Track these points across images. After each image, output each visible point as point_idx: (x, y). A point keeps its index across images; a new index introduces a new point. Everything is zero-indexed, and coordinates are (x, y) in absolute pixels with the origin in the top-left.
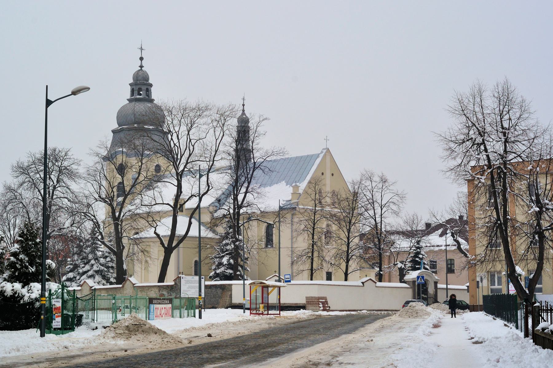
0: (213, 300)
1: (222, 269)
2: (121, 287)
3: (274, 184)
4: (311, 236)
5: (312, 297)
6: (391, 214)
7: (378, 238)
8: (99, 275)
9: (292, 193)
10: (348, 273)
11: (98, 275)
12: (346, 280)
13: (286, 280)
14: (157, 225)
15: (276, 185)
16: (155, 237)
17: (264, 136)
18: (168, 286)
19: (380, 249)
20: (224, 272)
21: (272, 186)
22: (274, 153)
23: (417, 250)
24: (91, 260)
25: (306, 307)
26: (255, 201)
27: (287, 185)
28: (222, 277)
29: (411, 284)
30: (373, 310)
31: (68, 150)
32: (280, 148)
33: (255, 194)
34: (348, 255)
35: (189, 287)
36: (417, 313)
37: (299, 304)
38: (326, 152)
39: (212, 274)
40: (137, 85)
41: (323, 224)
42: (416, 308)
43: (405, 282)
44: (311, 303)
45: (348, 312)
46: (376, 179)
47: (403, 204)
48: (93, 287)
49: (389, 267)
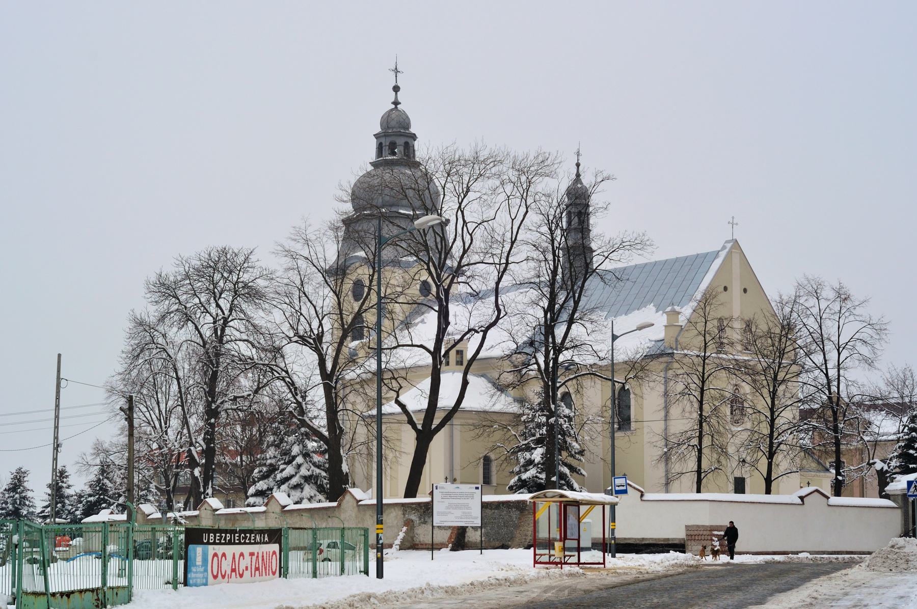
0: (504, 531)
1: (532, 472)
2: (335, 507)
3: (634, 310)
4: (696, 405)
5: (698, 526)
6: (857, 362)
7: (832, 408)
8: (311, 484)
9: (665, 326)
10: (773, 479)
11: (309, 484)
12: (768, 491)
13: (617, 488)
14: (401, 387)
15: (636, 311)
16: (399, 414)
17: (606, 212)
18: (419, 504)
19: (836, 429)
20: (536, 477)
21: (631, 313)
22: (624, 244)
23: (910, 433)
24: (296, 456)
25: (686, 547)
26: (590, 338)
27: (657, 311)
28: (532, 487)
29: (900, 501)
30: (824, 553)
31: (250, 251)
32: (635, 235)
33: (588, 325)
34: (771, 443)
35: (450, 506)
36: (907, 561)
37: (673, 539)
38: (732, 248)
39: (513, 481)
40: (388, 136)
41: (721, 383)
42: (906, 550)
43: (887, 497)
44: (697, 538)
45: (769, 557)
46: (828, 293)
47: (883, 342)
48: (286, 506)
49: (860, 470)
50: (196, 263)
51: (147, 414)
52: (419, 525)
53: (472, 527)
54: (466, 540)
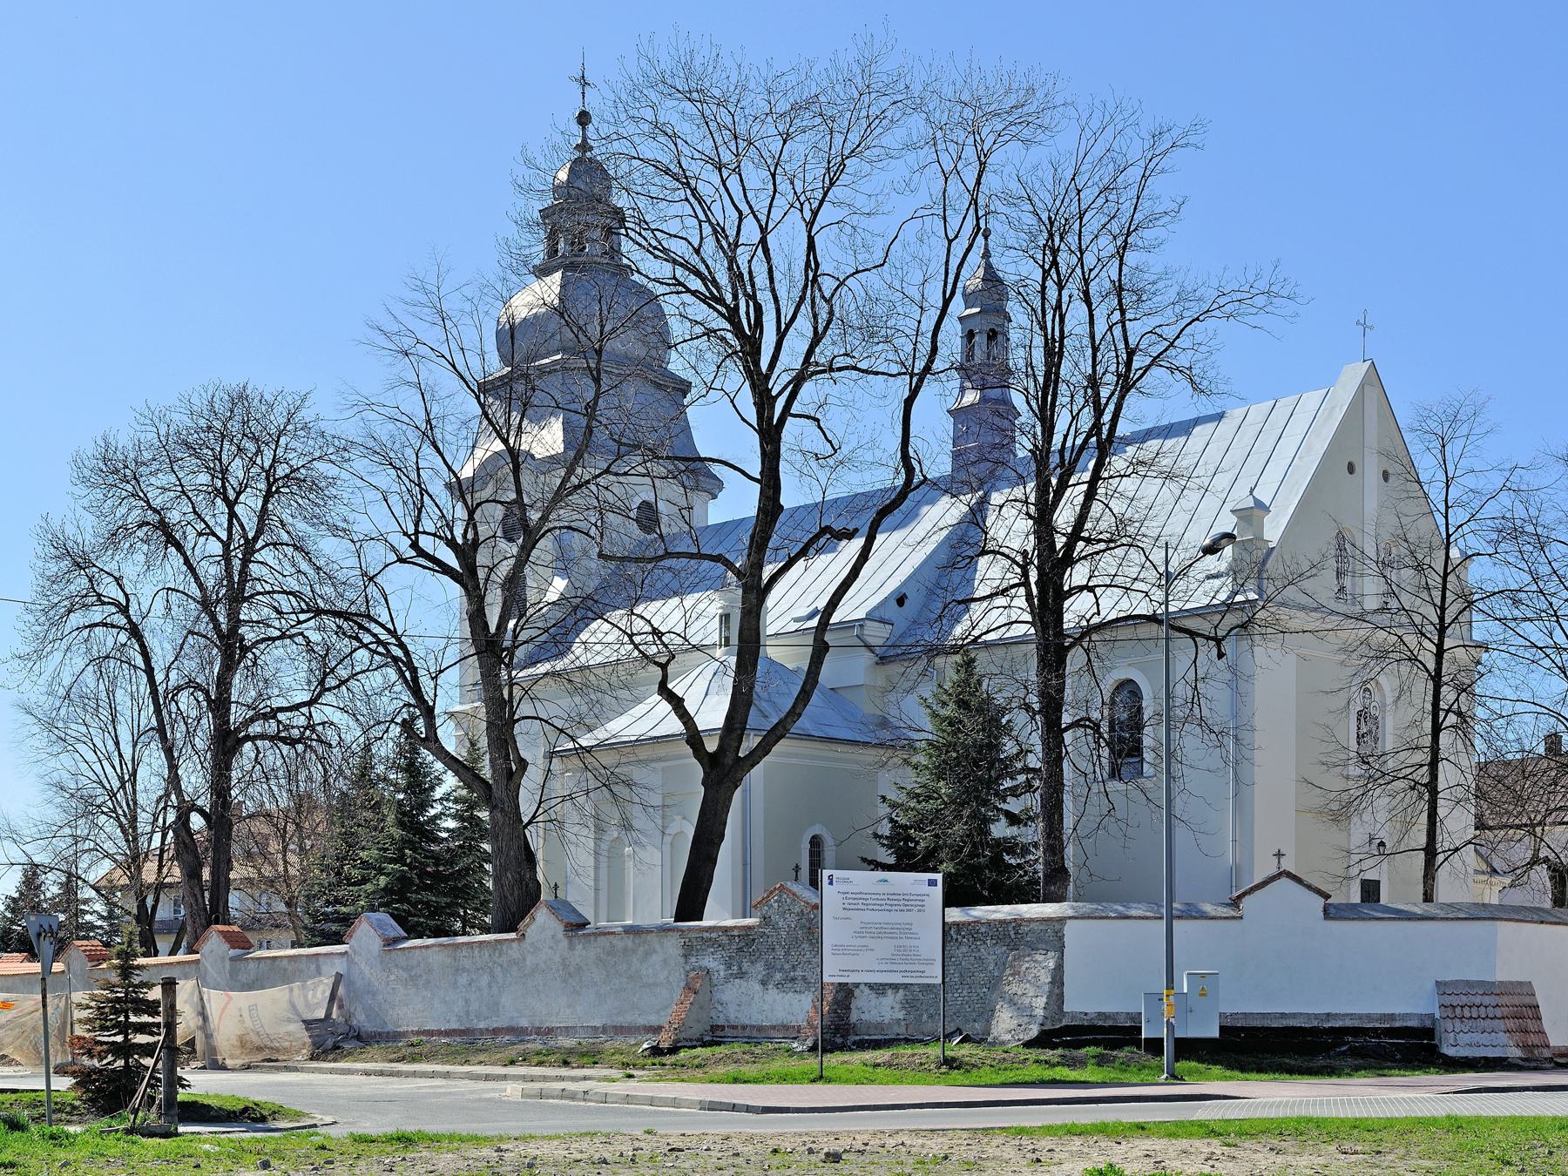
5: (1468, 983)
25: (1437, 1034)
44: (1467, 1014)
50: (181, 420)
51: (97, 767)
52: (726, 980)
53: (871, 986)
54: (854, 1018)
